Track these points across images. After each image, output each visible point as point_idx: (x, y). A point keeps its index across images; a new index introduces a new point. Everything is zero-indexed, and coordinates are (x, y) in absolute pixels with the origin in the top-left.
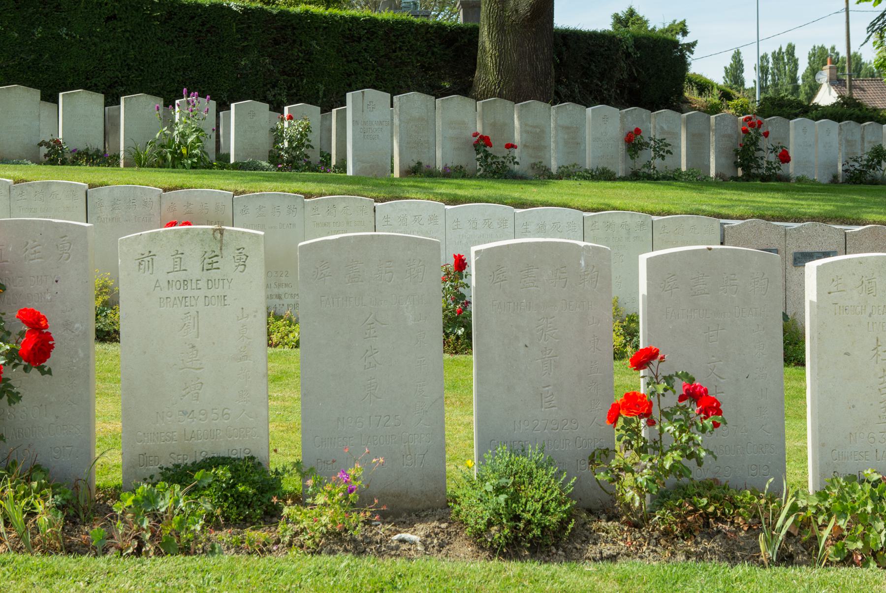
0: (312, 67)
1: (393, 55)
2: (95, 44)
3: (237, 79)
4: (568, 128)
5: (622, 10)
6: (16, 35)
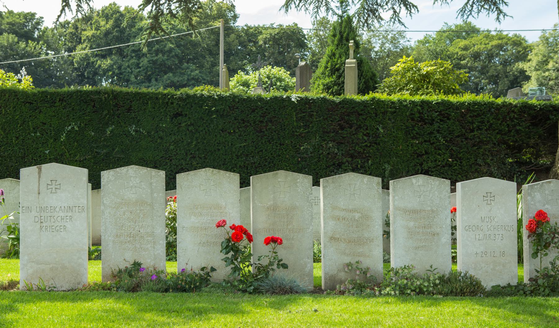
0: (378, 149)
1: (470, 135)
2: (161, 138)
3: (299, 162)
4: (415, 212)
5: (112, 2)
6: (93, 134)
